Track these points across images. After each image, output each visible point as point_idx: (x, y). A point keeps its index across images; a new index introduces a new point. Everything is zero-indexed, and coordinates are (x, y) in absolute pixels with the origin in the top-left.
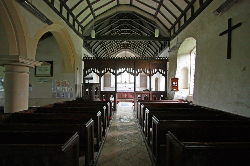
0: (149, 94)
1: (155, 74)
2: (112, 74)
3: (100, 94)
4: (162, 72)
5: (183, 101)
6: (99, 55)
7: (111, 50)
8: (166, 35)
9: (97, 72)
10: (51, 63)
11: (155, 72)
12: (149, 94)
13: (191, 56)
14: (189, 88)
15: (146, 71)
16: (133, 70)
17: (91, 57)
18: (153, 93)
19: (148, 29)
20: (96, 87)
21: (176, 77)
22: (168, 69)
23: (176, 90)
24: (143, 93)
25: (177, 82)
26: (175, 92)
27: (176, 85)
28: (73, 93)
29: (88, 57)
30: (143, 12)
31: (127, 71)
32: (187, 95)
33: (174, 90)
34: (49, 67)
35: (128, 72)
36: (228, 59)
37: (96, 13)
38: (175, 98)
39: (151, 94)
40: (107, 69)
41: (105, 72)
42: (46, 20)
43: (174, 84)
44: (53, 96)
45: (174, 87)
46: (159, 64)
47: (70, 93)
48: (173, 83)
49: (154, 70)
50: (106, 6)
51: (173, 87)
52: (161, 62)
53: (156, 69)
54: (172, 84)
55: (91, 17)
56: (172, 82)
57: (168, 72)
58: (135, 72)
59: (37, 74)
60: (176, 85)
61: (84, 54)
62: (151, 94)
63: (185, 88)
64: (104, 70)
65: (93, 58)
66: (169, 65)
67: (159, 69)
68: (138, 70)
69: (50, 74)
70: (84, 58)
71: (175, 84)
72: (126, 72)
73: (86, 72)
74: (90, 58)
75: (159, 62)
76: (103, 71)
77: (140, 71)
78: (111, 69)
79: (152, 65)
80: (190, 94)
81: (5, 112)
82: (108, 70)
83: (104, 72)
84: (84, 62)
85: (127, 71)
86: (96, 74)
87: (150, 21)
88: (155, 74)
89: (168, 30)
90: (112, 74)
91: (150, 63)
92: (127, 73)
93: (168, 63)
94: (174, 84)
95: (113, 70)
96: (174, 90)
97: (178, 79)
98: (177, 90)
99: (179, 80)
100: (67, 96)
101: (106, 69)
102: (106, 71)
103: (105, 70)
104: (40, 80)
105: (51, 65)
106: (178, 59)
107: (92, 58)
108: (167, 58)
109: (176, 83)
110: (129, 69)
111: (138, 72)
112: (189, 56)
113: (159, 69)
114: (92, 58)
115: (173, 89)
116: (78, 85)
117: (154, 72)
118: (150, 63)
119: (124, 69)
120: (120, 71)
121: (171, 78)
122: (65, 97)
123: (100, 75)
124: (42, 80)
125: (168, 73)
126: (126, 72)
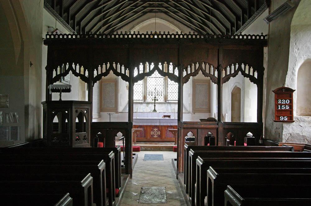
1: (232, 78)
2: (120, 77)
3: (90, 129)
4: (212, 73)
6: (87, 29)
12: (217, 129)
15: (207, 71)
16: (174, 69)
17: (65, 34)
18: (226, 127)
20: (79, 111)
21: (286, 86)
22: (265, 66)
23: (286, 119)
26: (285, 125)
29: (59, 33)
31: (201, 69)
41: (103, 72)
43: (281, 105)
47: (10, 128)
48: (280, 102)
51: (279, 113)
56: (277, 100)
57: (265, 72)
58: (180, 73)
61: (49, 27)
64: (99, 68)
65: (72, 36)
67: (243, 66)
68: (189, 69)
70: (48, 37)
71: (285, 105)
73: (95, 72)
74: (63, 36)
76: (97, 70)
78: (119, 65)
82: (240, 68)
83: (141, 72)
88: (232, 78)
90: (120, 77)
93: (266, 50)
94: (281, 105)
95: (123, 68)
96: (282, 118)
101: (104, 66)
102: (104, 71)
103: (103, 68)
106: (291, 40)
107: (70, 37)
108: (264, 37)
109: (288, 102)
111: (189, 72)
113: (243, 66)
114: (68, 36)
116: (32, 107)
117: (189, 72)
123: (90, 81)
126: (156, 72)
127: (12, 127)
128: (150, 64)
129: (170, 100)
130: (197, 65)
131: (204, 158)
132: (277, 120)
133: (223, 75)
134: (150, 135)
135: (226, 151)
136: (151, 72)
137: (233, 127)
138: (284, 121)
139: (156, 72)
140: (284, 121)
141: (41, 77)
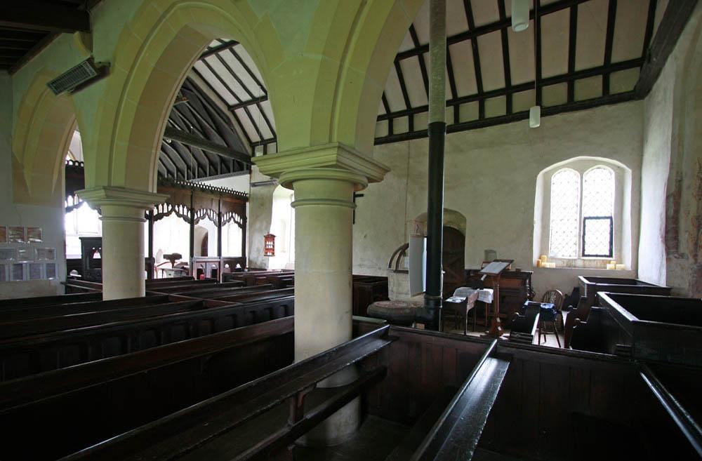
4: (185, 214)
12: (220, 262)
18: (226, 260)
19: (200, 97)
22: (247, 216)
23: (271, 254)
26: (270, 258)
27: (272, 247)
28: (56, 266)
31: (175, 211)
33: (268, 254)
35: (179, 215)
37: (240, 112)
41: (75, 204)
42: (400, 256)
45: (267, 249)
47: (45, 266)
48: (267, 243)
49: (163, 205)
51: (267, 250)
55: (255, 138)
56: (266, 242)
57: (248, 220)
58: (193, 216)
60: (272, 247)
66: (250, 208)
72: (174, 213)
84: (468, 266)
85: (175, 211)
86: (182, 218)
93: (247, 204)
97: (274, 236)
99: (275, 238)
110: (181, 208)
113: (209, 211)
119: (170, 208)
127: (48, 265)
133: (196, 217)
135: (682, 409)
136: (168, 214)
141: (614, 300)
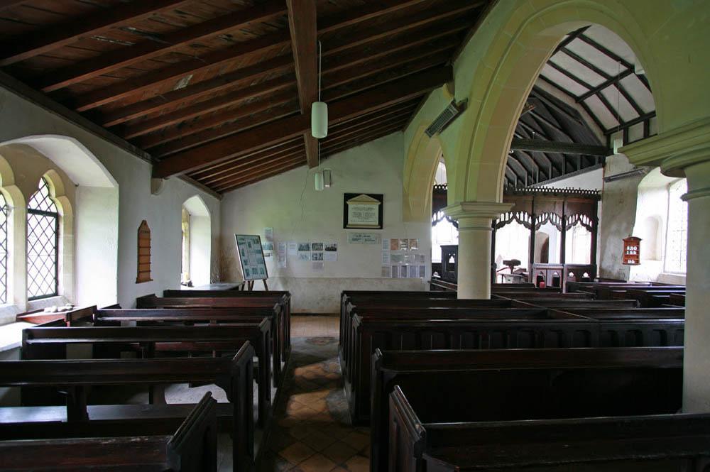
0: (560, 271)
1: (542, 226)
4: (558, 222)
5: (653, 284)
7: (300, 159)
8: (599, 141)
9: (588, 223)
10: (379, 198)
11: (507, 219)
13: (671, 194)
14: (663, 259)
15: (554, 221)
16: (528, 218)
21: (634, 235)
22: (599, 216)
23: (633, 262)
24: (551, 269)
25: (638, 244)
26: (632, 267)
27: (635, 253)
30: (553, 87)
31: (516, 218)
32: (659, 273)
33: (629, 262)
34: (375, 206)
35: (519, 221)
36: (681, 200)
38: (630, 280)
39: (565, 270)
40: (547, 215)
43: (629, 251)
44: (384, 273)
46: (583, 203)
48: (628, 248)
50: (582, 87)
51: (627, 257)
52: (586, 201)
53: (509, 213)
54: (625, 251)
56: (626, 247)
57: (600, 222)
58: (533, 221)
59: (349, 222)
60: (635, 253)
62: (565, 270)
63: (651, 259)
67: (581, 217)
68: (540, 218)
69: (377, 223)
71: (633, 251)
72: (514, 220)
75: (581, 201)
77: (543, 220)
79: (568, 207)
80: (664, 272)
81: (459, 297)
82: (549, 218)
87: (566, 109)
88: (542, 226)
89: (604, 132)
91: (564, 203)
92: (447, 222)
93: (600, 203)
94: (629, 251)
96: (629, 262)
97: (640, 240)
98: (637, 262)
99: (641, 242)
100: (413, 272)
104: (355, 237)
105: (380, 203)
106: (638, 199)
108: (597, 192)
109: (635, 248)
111: (540, 221)
112: (666, 192)
115: (627, 261)
117: (540, 221)
118: (564, 203)
120: (435, 219)
121: (624, 238)
122: (408, 275)
124: (360, 236)
125: (599, 226)
126: (514, 220)
128: (509, 213)
129: (40, 294)
130: (547, 215)
131: (384, 351)
132: (625, 262)
134: (440, 283)
137: (574, 268)
138: (631, 264)
139: (514, 220)
140: (631, 264)
